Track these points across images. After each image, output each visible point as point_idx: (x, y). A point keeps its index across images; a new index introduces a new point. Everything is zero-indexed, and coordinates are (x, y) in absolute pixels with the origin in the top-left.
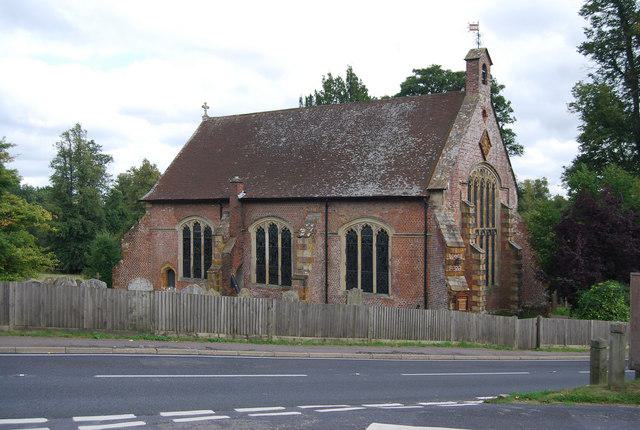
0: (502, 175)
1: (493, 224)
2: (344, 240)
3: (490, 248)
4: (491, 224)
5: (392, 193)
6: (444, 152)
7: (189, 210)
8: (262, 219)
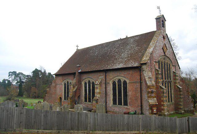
0: (173, 61)
1: (170, 79)
2: (112, 85)
3: (169, 88)
4: (169, 79)
5: (128, 66)
6: (147, 50)
7: (65, 77)
8: (86, 79)
